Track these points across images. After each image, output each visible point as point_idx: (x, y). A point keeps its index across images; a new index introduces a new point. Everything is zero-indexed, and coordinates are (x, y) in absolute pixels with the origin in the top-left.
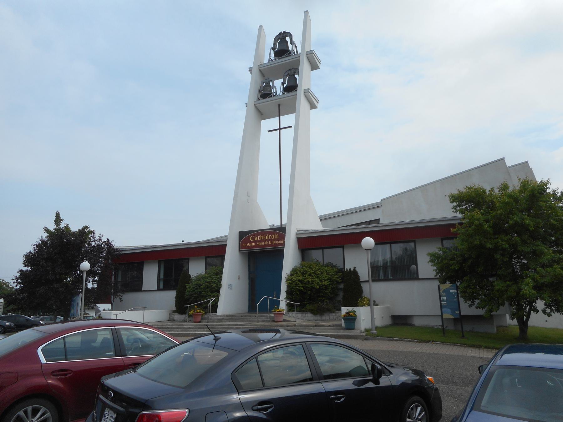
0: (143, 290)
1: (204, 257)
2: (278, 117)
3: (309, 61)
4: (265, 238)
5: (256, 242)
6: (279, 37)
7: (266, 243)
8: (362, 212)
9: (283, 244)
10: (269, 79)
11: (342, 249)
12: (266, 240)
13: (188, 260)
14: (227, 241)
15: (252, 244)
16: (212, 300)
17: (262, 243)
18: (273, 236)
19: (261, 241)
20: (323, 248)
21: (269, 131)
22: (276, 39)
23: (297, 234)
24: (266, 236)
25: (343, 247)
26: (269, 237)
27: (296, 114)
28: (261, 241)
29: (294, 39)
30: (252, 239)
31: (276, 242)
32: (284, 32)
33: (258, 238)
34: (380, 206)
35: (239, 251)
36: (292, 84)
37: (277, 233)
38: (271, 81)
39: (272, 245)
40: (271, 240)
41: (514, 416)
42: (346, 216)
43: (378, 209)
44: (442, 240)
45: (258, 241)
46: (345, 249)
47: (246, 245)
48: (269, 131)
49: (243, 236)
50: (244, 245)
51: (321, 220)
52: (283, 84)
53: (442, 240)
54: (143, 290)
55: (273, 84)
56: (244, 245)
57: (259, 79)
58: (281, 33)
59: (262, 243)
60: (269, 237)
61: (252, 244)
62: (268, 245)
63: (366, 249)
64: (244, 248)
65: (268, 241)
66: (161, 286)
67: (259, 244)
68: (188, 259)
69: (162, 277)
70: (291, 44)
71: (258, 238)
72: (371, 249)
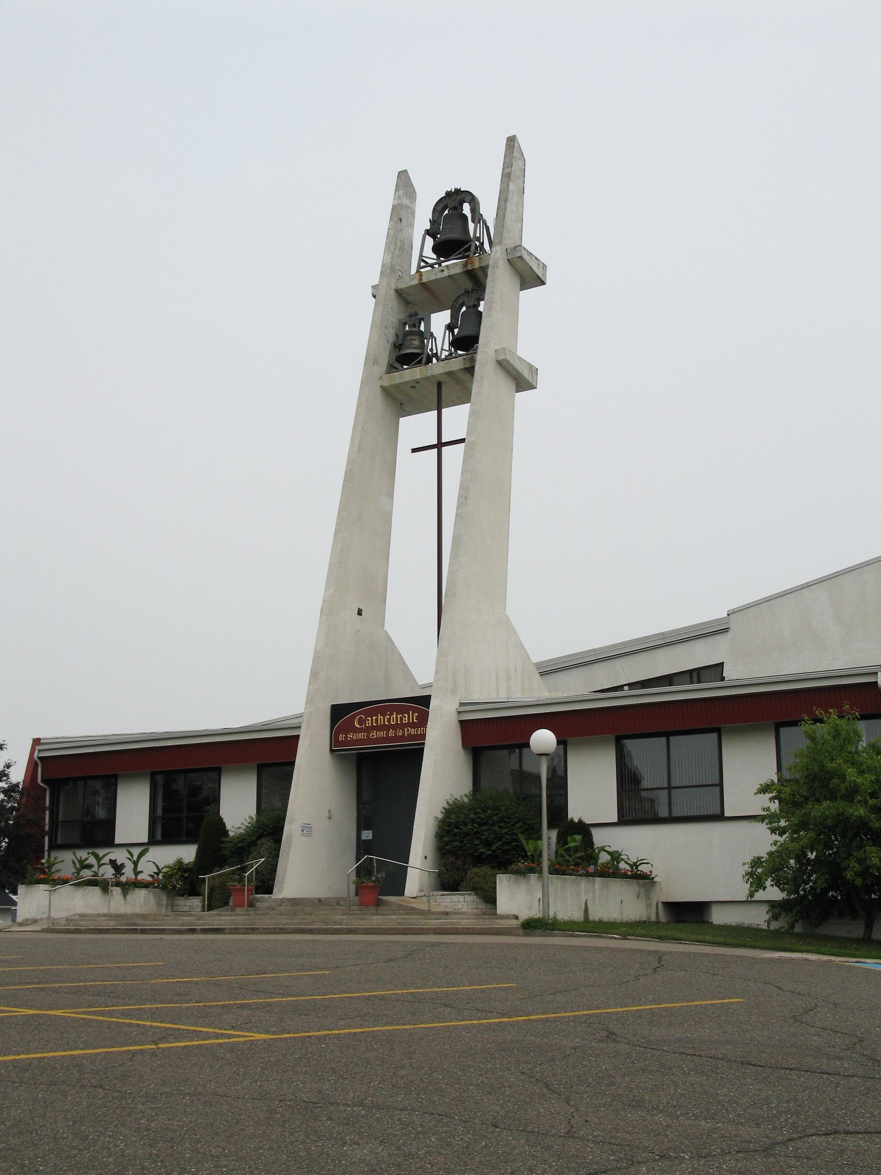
0: (116, 843)
1: (612, 737)
2: (436, 412)
3: (516, 269)
4: (389, 720)
5: (368, 730)
6: (446, 203)
7: (391, 733)
8: (632, 656)
9: (423, 736)
10: (417, 314)
11: (715, 736)
12: (390, 726)
13: (217, 772)
14: (300, 727)
15: (361, 736)
16: (257, 863)
17: (382, 734)
18: (405, 717)
19: (379, 728)
20: (668, 734)
21: (414, 450)
22: (440, 206)
23: (459, 712)
24: (391, 714)
25: (718, 731)
26: (397, 717)
27: (473, 414)
28: (379, 728)
29: (483, 210)
30: (360, 723)
31: (413, 731)
32: (458, 191)
33: (372, 720)
34: (726, 630)
35: (332, 751)
36: (469, 332)
37: (415, 710)
38: (423, 319)
39: (402, 739)
40: (402, 726)
41: (390, 929)
42: (656, 651)
43: (720, 638)
44: (778, 726)
45: (372, 728)
46: (723, 736)
47: (346, 737)
48: (414, 450)
49: (339, 712)
50: (341, 737)
51: (542, 674)
52: (450, 328)
53: (778, 726)
54: (116, 843)
55: (428, 326)
56: (341, 737)
57: (395, 312)
58: (449, 194)
59: (382, 734)
60: (397, 717)
61: (361, 736)
62: (396, 738)
63: (538, 754)
64: (343, 743)
65: (396, 727)
66: (159, 836)
67: (374, 734)
68: (218, 771)
69: (160, 813)
70: (473, 221)
71: (372, 720)
72: (549, 754)
